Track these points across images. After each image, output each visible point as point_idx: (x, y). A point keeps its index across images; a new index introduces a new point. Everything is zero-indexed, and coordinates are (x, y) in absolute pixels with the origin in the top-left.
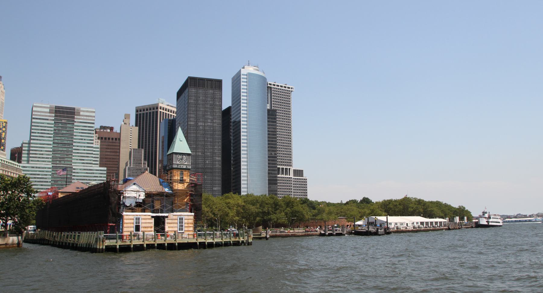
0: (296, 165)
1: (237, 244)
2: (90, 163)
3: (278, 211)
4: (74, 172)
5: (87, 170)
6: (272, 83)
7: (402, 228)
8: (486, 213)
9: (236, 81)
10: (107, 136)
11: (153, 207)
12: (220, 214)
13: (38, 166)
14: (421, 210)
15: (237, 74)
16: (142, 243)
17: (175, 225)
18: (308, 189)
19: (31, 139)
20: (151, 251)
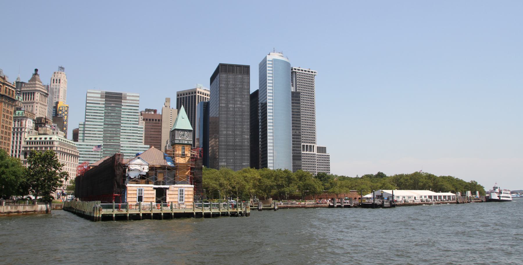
0: (319, 143)
1: (233, 215)
2: (136, 142)
3: (291, 185)
4: (122, 150)
5: (133, 147)
6: (297, 68)
7: (410, 201)
8: (497, 188)
9: (263, 66)
10: (151, 118)
11: (156, 179)
12: (237, 187)
13: (91, 144)
14: (431, 185)
15: (263, 60)
16: (138, 212)
17: (176, 196)
18: (331, 164)
19: (86, 121)
20: (147, 222)
